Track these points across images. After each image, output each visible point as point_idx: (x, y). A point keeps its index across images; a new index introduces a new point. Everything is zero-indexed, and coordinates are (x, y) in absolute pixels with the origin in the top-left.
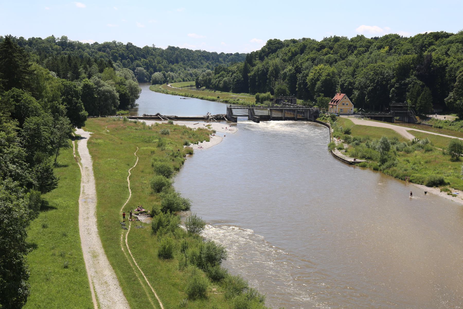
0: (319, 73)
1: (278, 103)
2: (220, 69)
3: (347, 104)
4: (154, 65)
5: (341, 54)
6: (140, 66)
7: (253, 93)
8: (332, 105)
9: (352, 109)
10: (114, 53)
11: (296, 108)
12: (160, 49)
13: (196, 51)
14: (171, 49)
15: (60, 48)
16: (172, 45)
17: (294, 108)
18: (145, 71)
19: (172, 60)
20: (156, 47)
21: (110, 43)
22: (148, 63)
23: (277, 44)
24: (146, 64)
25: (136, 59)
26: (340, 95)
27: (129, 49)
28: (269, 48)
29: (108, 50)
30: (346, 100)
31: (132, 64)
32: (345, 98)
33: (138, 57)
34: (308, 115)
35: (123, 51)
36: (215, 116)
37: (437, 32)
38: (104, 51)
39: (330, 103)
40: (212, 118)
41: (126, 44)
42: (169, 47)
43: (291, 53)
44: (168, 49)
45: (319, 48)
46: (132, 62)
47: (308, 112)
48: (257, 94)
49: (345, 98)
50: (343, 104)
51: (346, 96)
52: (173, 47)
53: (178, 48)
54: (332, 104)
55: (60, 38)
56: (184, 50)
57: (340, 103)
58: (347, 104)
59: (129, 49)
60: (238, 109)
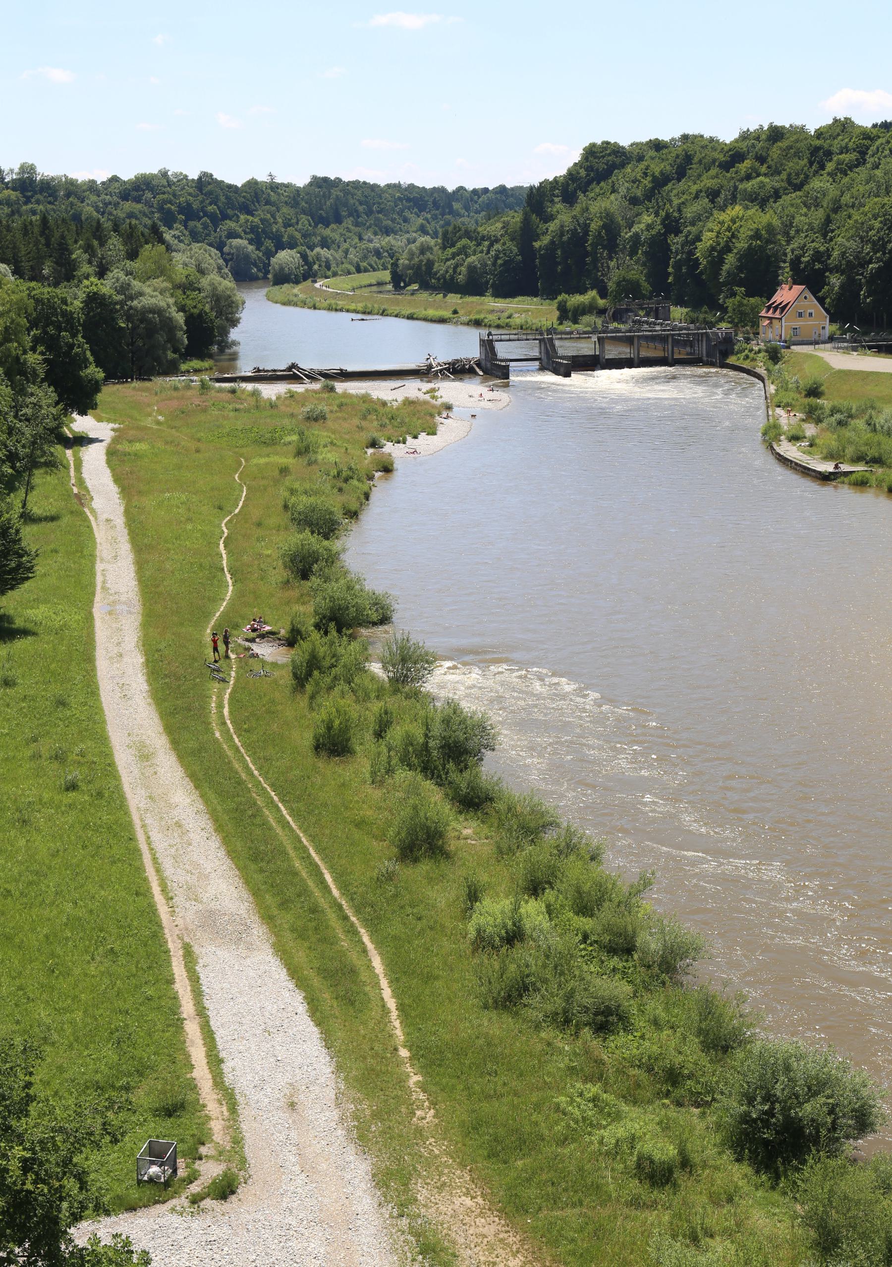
0: (729, 229)
1: (621, 319)
2: (456, 233)
3: (811, 314)
4: (274, 230)
5: (789, 175)
6: (241, 238)
7: (550, 294)
8: (770, 318)
9: (823, 328)
10: (165, 202)
11: (668, 330)
12: (288, 186)
13: (389, 186)
14: (321, 184)
15: (17, 197)
16: (321, 174)
17: (664, 330)
18: (251, 248)
19: (324, 215)
20: (279, 180)
21: (153, 176)
22: (257, 227)
23: (609, 155)
24: (253, 229)
25: (225, 217)
26: (790, 289)
27: (205, 190)
28: (589, 169)
29: (148, 195)
30: (806, 303)
31: (215, 231)
32: (806, 298)
33: (230, 212)
34: (704, 347)
35: (189, 197)
36: (449, 364)
37: (836, 121)
38: (138, 200)
39: (763, 313)
40: (441, 371)
41: (196, 178)
42: (315, 178)
43: (649, 178)
44: (311, 184)
45: (726, 162)
46: (216, 226)
47: (702, 341)
48: (560, 298)
49: (806, 298)
50: (800, 315)
51: (807, 291)
52: (326, 180)
53: (338, 181)
54: (770, 314)
55: (16, 170)
56: (356, 185)
57: (790, 312)
58: (811, 314)
59: (205, 190)
60: (510, 340)
